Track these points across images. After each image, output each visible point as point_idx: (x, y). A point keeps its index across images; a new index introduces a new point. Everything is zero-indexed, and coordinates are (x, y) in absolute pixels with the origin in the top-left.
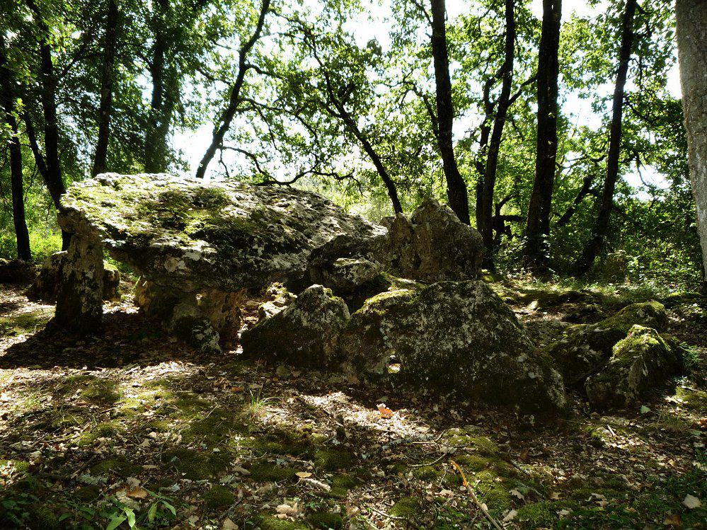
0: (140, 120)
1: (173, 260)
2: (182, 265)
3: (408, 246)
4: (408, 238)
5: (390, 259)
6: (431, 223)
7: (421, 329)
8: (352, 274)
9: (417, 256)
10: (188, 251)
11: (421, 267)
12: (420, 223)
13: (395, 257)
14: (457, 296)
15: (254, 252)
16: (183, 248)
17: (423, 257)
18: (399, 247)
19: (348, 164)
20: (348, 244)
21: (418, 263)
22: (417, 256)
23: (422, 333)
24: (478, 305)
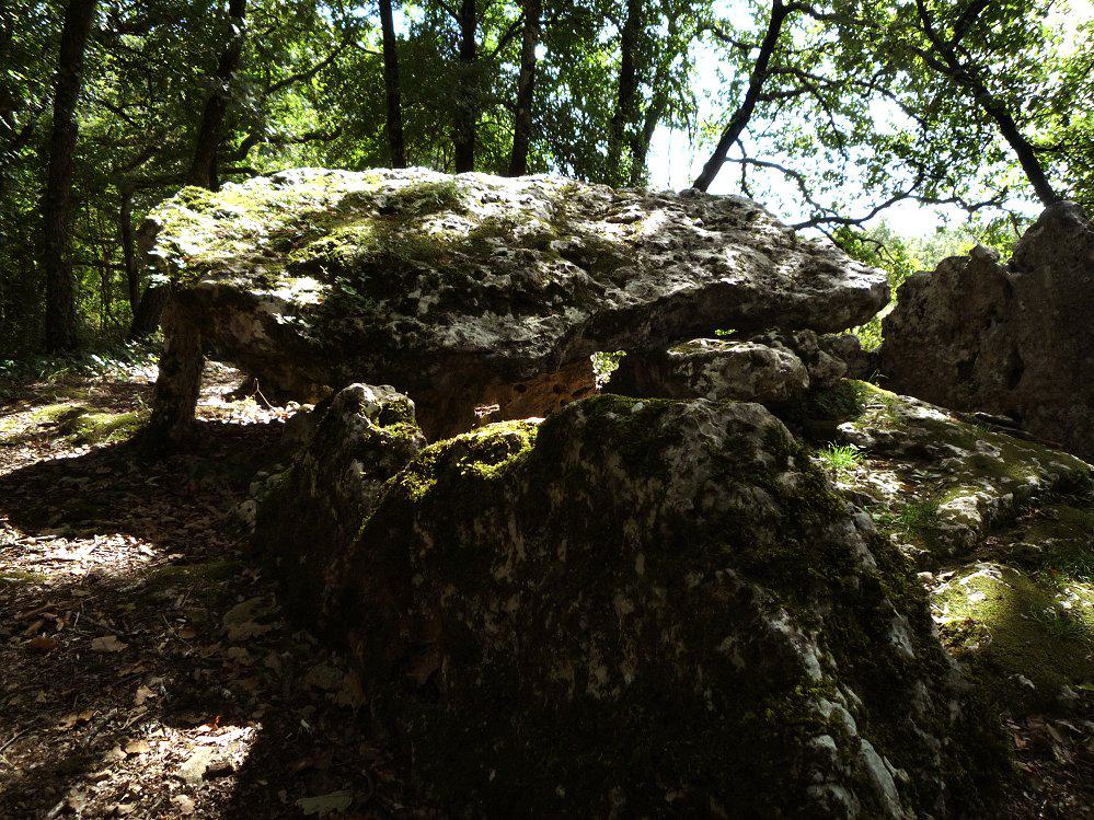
0: (282, 36)
1: (242, 317)
2: (258, 330)
3: (995, 329)
4: (1000, 310)
5: (953, 360)
6: (1055, 267)
7: (503, 572)
8: (707, 379)
9: (1015, 355)
10: (265, 298)
11: (1025, 380)
12: (1032, 269)
13: (964, 355)
14: (614, 461)
15: (410, 307)
16: (258, 292)
17: (1027, 357)
18: (976, 333)
19: (996, 179)
20: (745, 308)
21: (1015, 373)
22: (1015, 355)
23: (504, 590)
24: (673, 516)
